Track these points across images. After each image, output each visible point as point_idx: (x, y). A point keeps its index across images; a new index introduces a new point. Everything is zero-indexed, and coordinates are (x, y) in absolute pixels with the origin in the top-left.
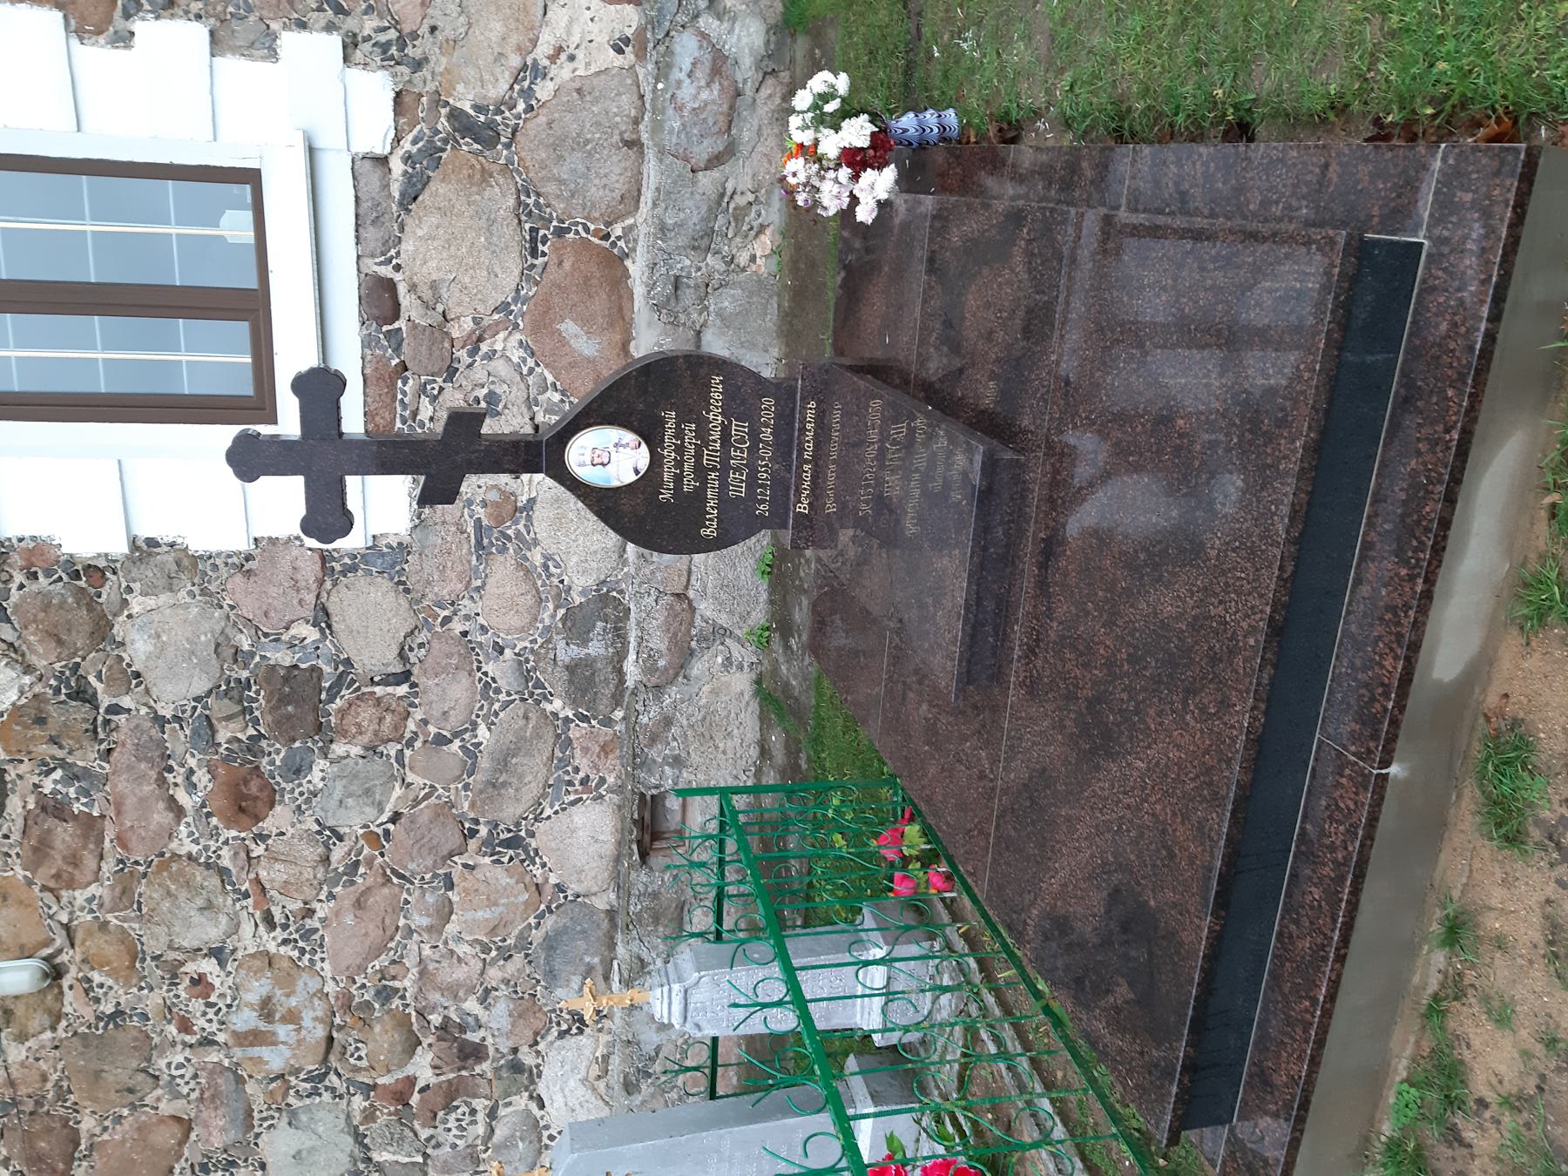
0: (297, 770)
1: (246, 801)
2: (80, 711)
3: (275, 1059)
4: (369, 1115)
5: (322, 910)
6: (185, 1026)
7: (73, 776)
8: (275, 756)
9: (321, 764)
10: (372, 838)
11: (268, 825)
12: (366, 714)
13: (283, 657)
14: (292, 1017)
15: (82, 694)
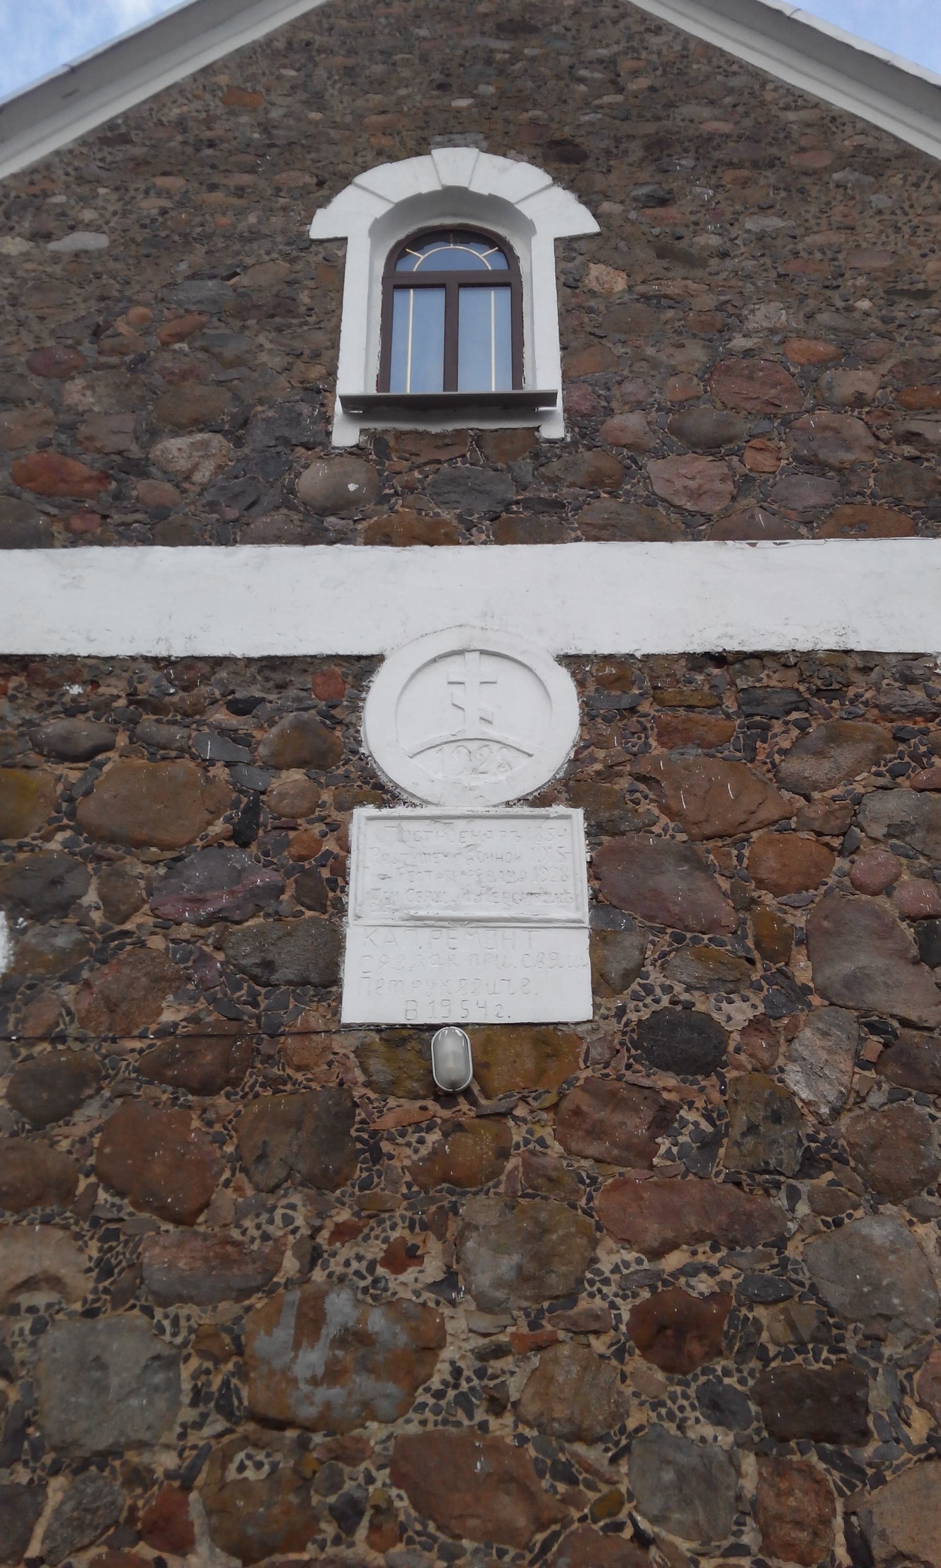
0: (717, 1406)
1: (671, 1332)
2: (790, 1158)
3: (271, 1341)
4: (139, 1477)
5: (502, 1427)
6: (343, 1233)
7: (708, 1144)
8: (732, 1376)
9: (726, 1439)
10: (612, 1504)
11: (636, 1362)
12: (801, 1500)
13: (878, 1394)
14: (333, 1374)
15: (810, 1164)
